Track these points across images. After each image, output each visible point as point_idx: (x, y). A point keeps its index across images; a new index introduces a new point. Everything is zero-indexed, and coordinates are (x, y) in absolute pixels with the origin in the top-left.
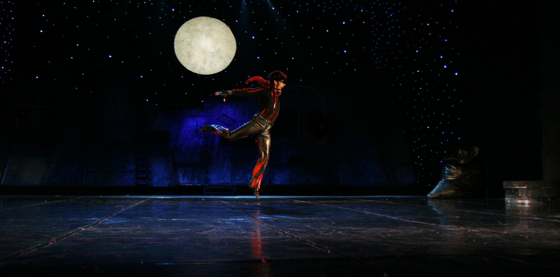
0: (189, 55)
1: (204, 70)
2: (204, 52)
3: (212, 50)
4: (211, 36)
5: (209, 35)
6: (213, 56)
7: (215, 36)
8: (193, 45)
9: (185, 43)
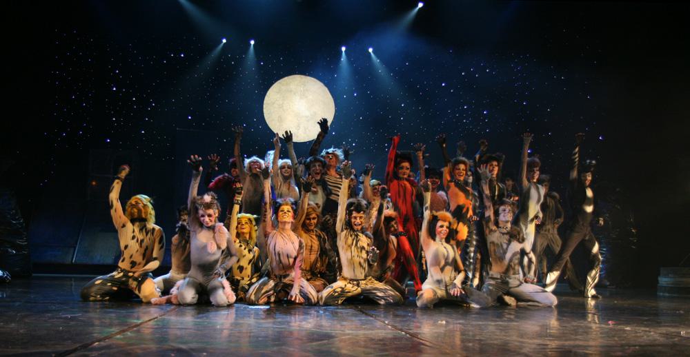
3: (307, 113)
4: (307, 97)
6: (308, 121)
7: (310, 97)
8: (285, 108)
9: (275, 105)
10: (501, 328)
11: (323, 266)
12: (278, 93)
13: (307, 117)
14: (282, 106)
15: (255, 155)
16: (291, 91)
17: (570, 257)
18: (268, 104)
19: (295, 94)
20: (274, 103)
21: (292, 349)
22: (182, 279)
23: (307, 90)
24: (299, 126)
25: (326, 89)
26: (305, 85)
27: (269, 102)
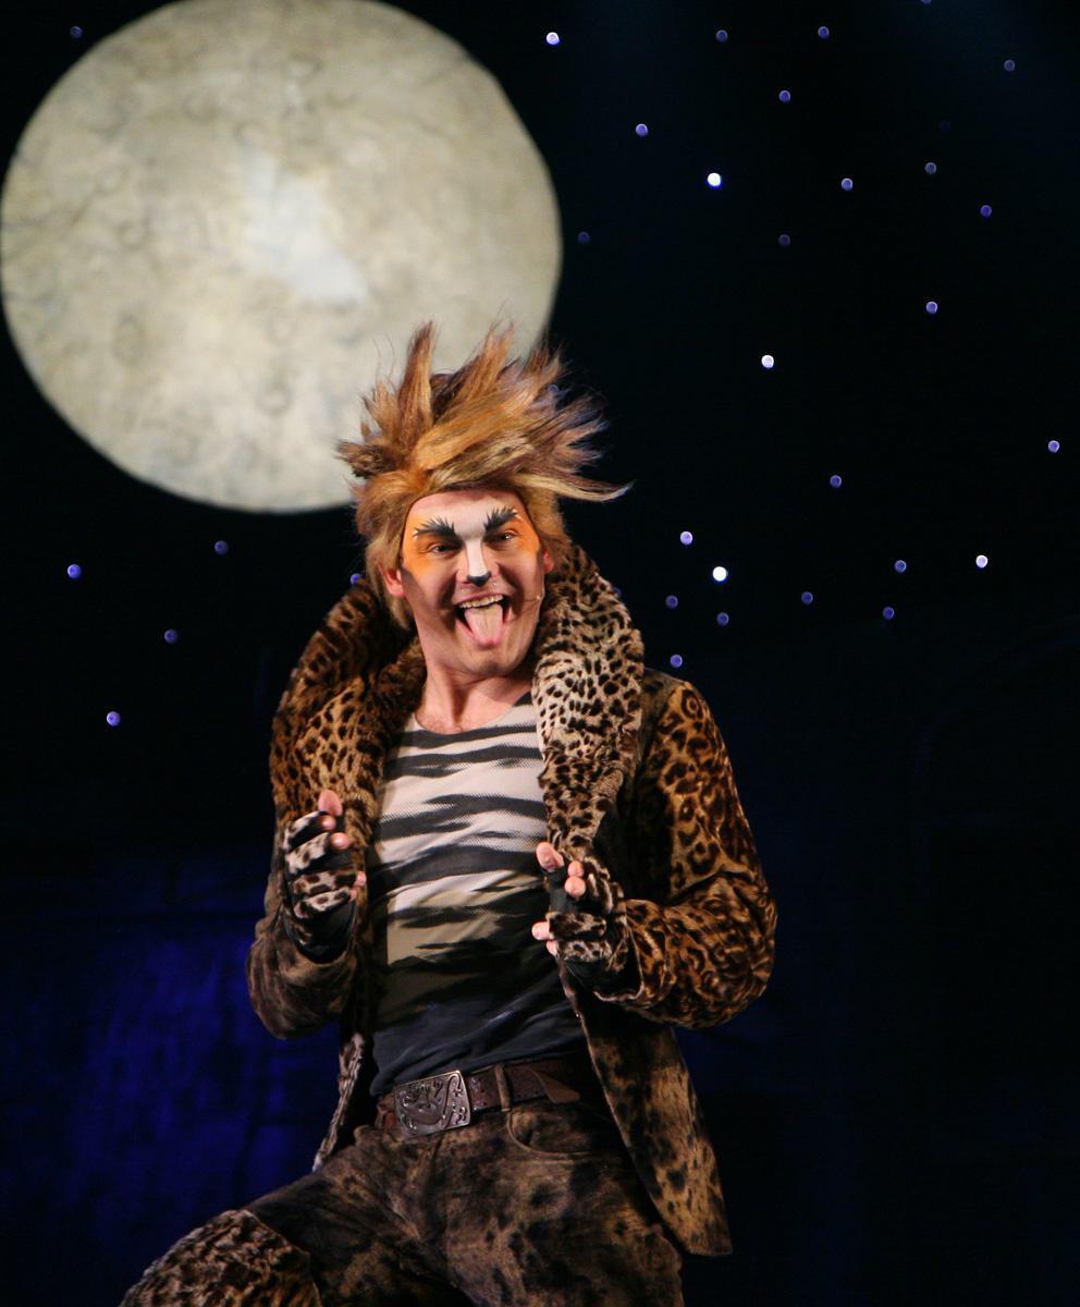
0: (138, 341)
1: (274, 469)
2: (268, 303)
3: (344, 283)
4: (331, 157)
5: (305, 147)
7: (363, 155)
8: (166, 248)
9: (94, 233)
10: (528, 1060)
11: (583, 653)
12: (110, 133)
13: (342, 309)
14: (148, 236)
15: (322, 913)
16: (209, 115)
17: (377, 1071)
18: (38, 224)
19: (238, 130)
20: (77, 216)
21: (476, 1221)
22: (161, 1270)
23: (334, 103)
24: (279, 386)
25: (484, 90)
26: (318, 66)
27: (42, 207)
